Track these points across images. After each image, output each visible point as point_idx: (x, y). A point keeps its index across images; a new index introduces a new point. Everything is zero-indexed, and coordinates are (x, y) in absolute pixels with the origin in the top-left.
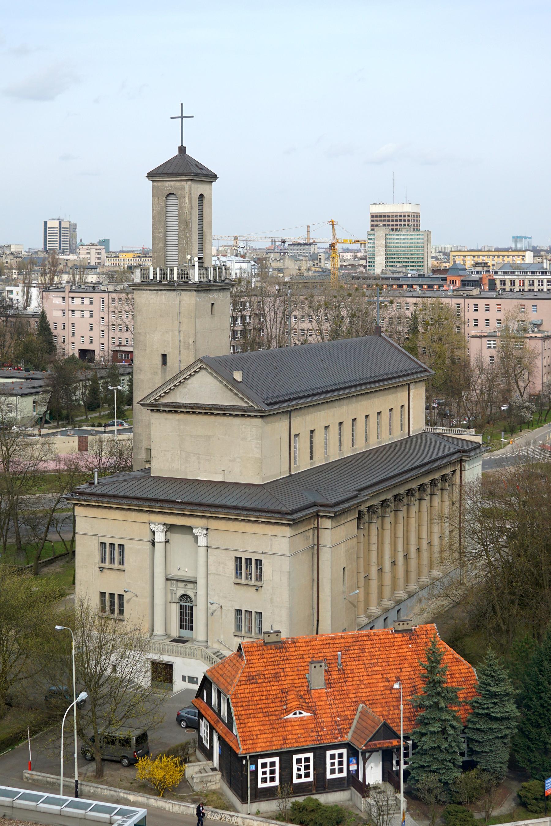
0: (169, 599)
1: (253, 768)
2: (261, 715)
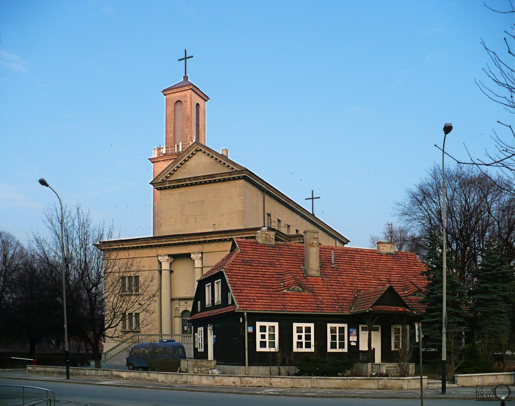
0: (174, 315)
1: (250, 329)
2: (258, 287)
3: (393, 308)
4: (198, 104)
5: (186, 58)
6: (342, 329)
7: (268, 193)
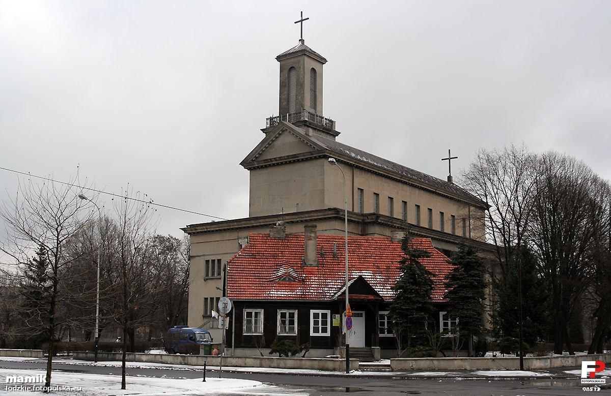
3: (363, 297)
4: (313, 70)
5: (302, 21)
6: (325, 316)
7: (358, 167)
